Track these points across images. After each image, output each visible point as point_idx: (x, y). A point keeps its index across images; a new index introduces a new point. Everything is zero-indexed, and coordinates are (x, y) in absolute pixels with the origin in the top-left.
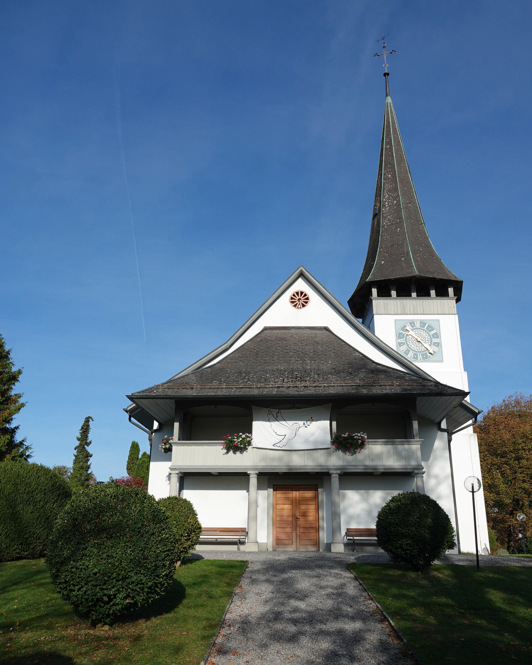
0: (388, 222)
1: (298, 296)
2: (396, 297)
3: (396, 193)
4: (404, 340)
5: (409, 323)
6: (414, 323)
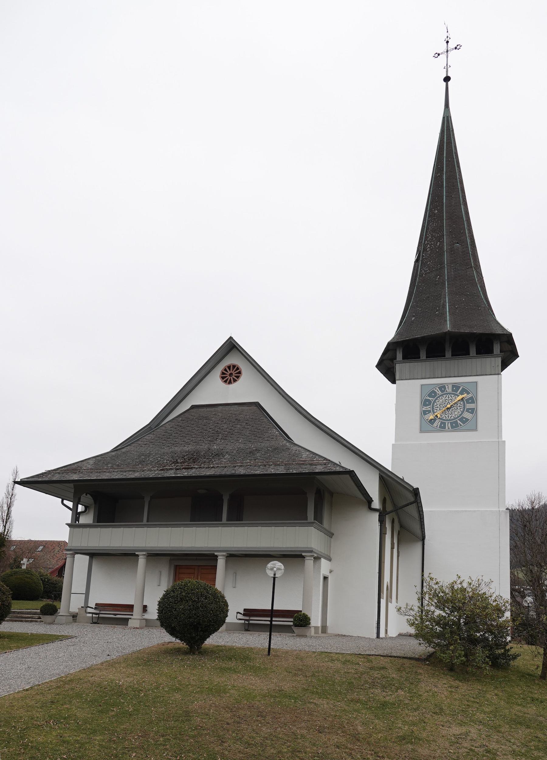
0: (427, 269)
1: (230, 371)
2: (451, 357)
3: (440, 232)
4: (430, 407)
5: (439, 388)
6: (444, 387)
